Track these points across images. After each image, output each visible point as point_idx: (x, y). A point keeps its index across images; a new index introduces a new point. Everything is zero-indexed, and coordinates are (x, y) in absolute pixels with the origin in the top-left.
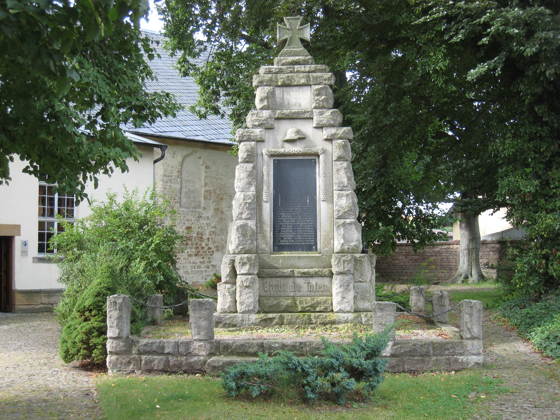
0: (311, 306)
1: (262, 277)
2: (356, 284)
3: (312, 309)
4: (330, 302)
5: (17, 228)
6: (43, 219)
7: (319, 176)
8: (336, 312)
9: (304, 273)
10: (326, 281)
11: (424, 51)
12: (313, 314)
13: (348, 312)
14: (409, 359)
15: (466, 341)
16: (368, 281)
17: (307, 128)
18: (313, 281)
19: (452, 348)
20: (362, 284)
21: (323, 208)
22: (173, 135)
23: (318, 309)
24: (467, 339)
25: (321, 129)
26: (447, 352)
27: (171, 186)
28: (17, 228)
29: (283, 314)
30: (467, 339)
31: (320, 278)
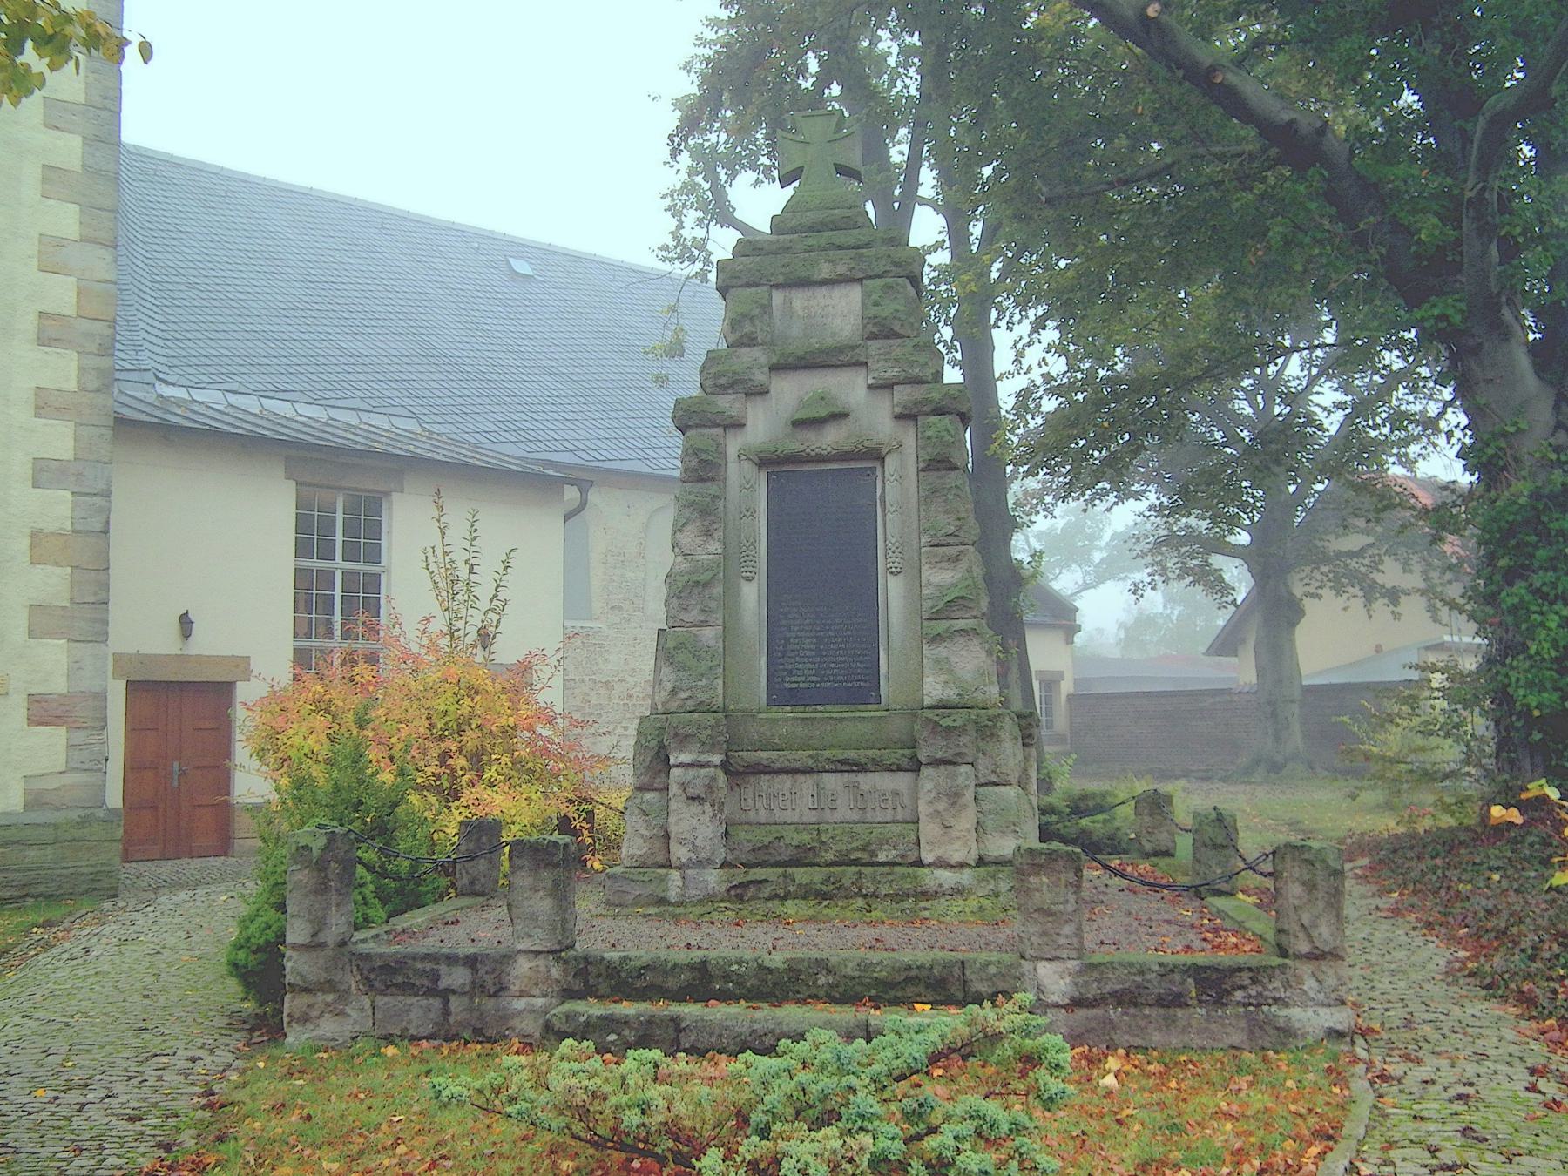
0: (863, 849)
1: (737, 773)
2: (981, 790)
3: (865, 857)
4: (913, 837)
5: (242, 665)
6: (304, 643)
7: (884, 510)
8: (929, 865)
9: (842, 762)
10: (901, 781)
11: (1045, 835)
12: (868, 870)
13: (961, 865)
14: (1126, 1014)
15: (1298, 964)
16: (1014, 779)
17: (851, 388)
18: (866, 781)
19: (1254, 981)
20: (997, 789)
21: (893, 593)
22: (625, 466)
23: (882, 857)
24: (1298, 956)
25: (886, 393)
26: (1239, 995)
27: (622, 576)
28: (1061, 674)
29: (789, 870)
30: (1298, 956)
31: (887, 774)
